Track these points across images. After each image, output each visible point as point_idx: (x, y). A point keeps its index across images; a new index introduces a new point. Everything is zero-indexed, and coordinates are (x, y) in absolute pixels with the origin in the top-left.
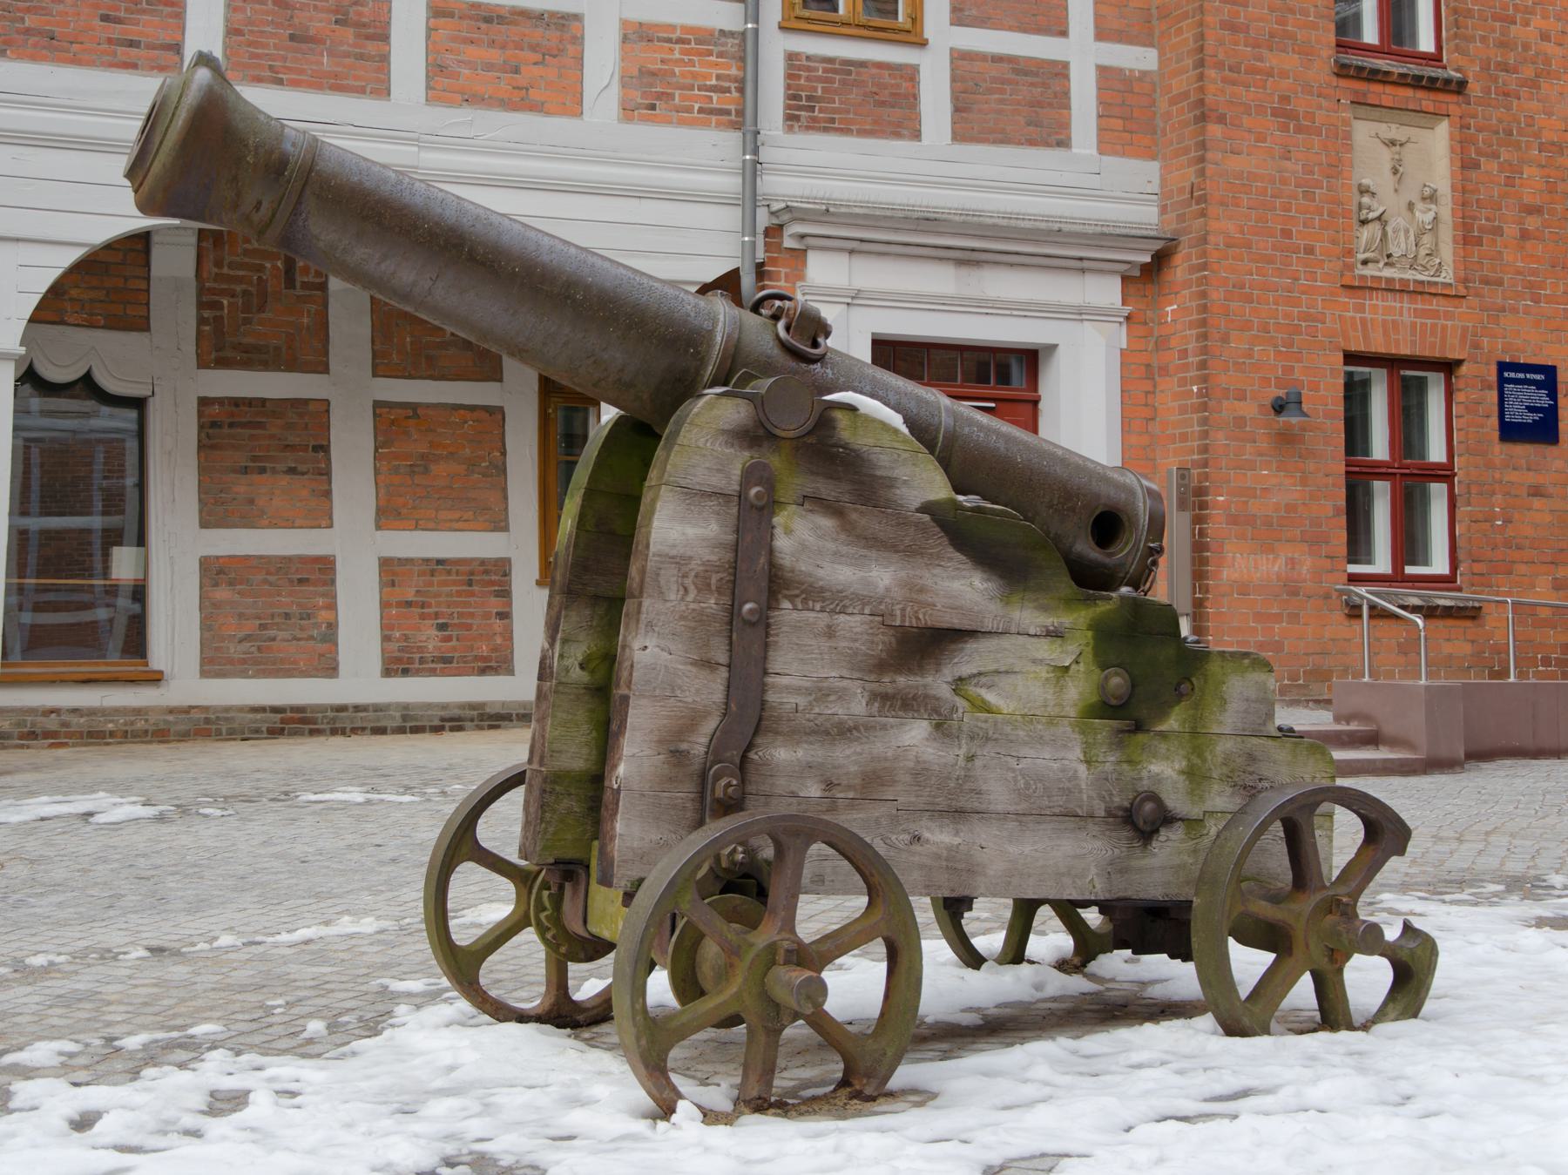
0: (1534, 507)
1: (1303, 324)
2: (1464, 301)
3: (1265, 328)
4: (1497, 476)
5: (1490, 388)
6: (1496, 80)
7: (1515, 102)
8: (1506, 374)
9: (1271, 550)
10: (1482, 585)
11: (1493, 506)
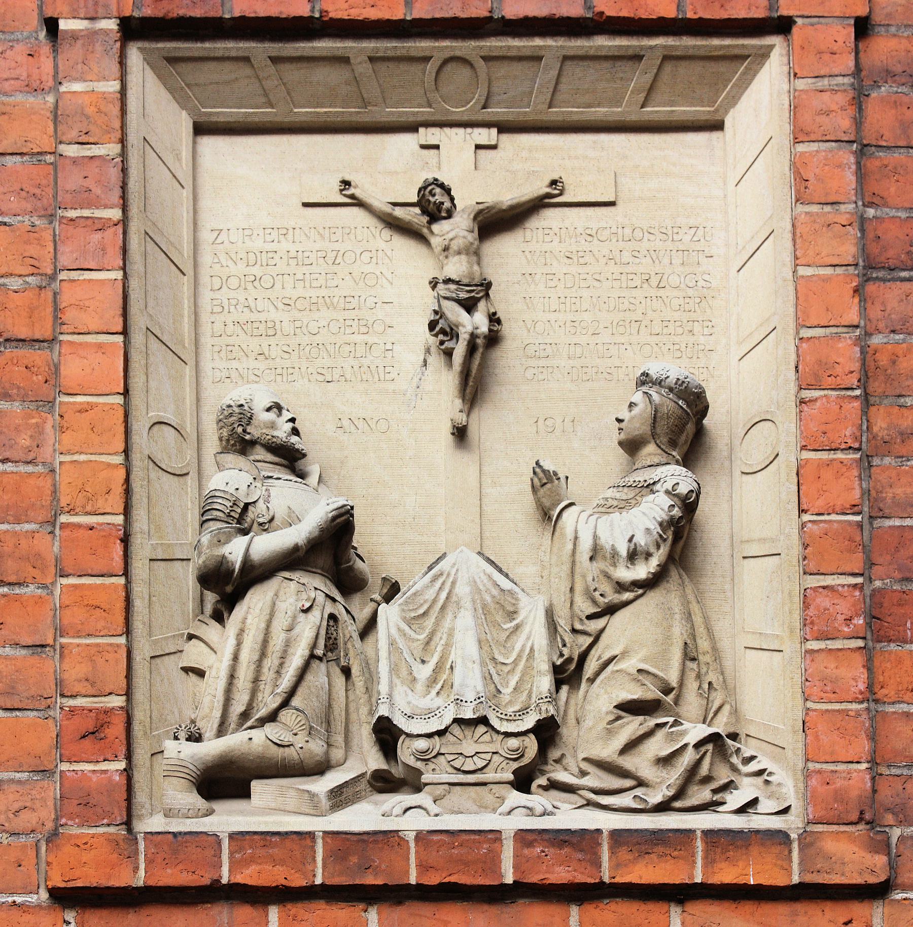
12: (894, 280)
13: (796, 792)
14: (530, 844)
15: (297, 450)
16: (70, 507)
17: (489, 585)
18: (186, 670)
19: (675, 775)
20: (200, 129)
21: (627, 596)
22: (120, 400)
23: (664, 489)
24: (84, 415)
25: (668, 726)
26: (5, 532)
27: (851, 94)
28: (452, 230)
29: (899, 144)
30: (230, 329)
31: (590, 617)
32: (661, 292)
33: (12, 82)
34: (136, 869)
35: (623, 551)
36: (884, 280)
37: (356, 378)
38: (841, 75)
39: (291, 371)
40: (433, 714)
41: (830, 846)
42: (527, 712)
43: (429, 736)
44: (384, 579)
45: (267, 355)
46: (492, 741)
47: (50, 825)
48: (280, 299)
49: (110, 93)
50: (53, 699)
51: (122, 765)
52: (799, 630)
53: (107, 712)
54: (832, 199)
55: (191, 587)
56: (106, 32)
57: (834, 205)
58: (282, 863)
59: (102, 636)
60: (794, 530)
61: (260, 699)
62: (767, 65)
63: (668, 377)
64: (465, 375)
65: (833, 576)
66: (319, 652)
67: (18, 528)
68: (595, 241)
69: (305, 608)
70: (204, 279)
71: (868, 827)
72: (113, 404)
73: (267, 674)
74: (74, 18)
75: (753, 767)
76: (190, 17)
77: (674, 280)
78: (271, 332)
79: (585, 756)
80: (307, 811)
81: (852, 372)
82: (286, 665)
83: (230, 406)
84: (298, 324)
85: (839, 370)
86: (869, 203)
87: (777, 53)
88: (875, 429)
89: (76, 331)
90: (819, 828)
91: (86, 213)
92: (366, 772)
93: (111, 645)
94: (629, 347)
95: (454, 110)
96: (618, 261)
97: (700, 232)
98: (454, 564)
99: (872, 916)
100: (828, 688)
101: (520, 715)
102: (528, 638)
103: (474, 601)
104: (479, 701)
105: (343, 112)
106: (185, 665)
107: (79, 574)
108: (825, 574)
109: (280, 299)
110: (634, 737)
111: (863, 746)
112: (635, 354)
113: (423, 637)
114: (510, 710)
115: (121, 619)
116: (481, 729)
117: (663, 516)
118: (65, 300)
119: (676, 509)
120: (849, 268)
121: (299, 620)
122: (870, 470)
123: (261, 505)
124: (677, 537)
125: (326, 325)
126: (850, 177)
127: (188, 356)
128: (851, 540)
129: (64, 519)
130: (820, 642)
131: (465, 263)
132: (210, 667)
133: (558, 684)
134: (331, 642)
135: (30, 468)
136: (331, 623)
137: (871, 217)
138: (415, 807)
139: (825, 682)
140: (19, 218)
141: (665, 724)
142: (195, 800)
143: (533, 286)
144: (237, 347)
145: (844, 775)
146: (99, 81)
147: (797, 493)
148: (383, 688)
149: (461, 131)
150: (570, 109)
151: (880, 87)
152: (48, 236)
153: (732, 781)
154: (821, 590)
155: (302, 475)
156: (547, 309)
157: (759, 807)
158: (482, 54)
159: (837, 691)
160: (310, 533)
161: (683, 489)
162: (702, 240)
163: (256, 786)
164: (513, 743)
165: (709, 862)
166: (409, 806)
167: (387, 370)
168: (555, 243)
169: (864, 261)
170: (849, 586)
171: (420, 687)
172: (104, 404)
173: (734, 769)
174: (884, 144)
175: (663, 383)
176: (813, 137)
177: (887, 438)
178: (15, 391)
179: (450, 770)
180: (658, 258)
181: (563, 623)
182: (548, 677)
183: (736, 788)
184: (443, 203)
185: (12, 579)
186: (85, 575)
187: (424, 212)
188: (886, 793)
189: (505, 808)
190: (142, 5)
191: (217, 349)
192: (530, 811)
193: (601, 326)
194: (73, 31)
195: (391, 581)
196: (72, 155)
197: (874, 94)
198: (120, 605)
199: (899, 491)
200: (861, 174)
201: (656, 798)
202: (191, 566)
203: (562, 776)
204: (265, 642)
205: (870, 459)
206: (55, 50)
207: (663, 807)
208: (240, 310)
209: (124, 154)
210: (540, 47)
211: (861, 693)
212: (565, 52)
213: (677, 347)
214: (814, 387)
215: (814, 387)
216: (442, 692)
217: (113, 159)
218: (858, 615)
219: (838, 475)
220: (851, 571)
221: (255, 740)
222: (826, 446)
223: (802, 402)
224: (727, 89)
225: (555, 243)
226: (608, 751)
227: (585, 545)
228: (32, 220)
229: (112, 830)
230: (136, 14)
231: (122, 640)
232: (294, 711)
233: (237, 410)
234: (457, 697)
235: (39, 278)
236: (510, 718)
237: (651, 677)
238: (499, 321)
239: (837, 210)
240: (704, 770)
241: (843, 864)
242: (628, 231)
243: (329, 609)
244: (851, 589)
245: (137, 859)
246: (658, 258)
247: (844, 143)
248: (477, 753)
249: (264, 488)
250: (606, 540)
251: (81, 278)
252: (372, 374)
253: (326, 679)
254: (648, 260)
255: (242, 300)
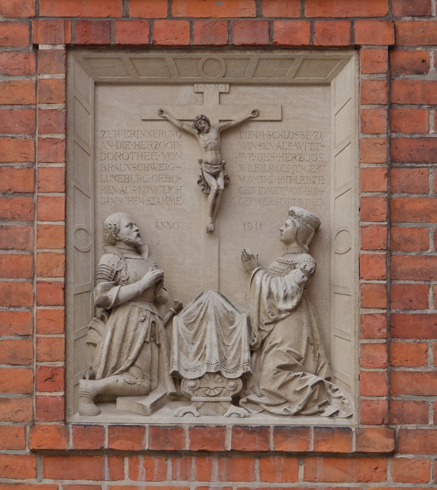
12: (403, 167)
13: (355, 408)
14: (238, 433)
15: (139, 244)
16: (42, 273)
17: (222, 309)
18: (88, 343)
20: (96, 84)
21: (283, 315)
23: (300, 267)
24: (47, 230)
25: (300, 377)
26: (12, 282)
27: (386, 82)
28: (209, 140)
29: (407, 103)
30: (109, 178)
31: (266, 324)
32: (301, 163)
33: (17, 71)
34: (68, 441)
35: (282, 295)
36: (399, 167)
37: (164, 203)
38: (382, 73)
39: (135, 199)
40: (197, 369)
41: (370, 435)
42: (238, 369)
43: (195, 379)
44: (176, 302)
45: (125, 191)
46: (223, 381)
48: (131, 165)
49: (61, 79)
50: (32, 360)
51: (62, 394)
52: (358, 333)
54: (377, 132)
55: (91, 304)
56: (59, 51)
57: (378, 135)
59: (54, 334)
60: (357, 285)
61: (121, 361)
62: (349, 63)
63: (303, 215)
64: (214, 207)
65: (373, 309)
66: (148, 340)
67: (18, 280)
68: (272, 138)
69: (142, 320)
71: (386, 426)
72: (60, 225)
73: (124, 349)
74: (46, 44)
76: (96, 44)
78: (127, 180)
79: (263, 388)
80: (141, 413)
81: (384, 214)
82: (133, 346)
83: (110, 224)
84: (139, 177)
85: (378, 212)
86: (393, 130)
87: (354, 59)
88: (394, 238)
89: (44, 191)
91: (50, 136)
92: (167, 393)
93: (58, 338)
94: (286, 189)
95: (210, 78)
96: (282, 148)
97: (319, 135)
98: (207, 299)
99: (387, 465)
100: (370, 362)
101: (235, 370)
102: (239, 334)
103: (215, 316)
104: (217, 364)
105: (161, 78)
106: (88, 341)
107: (44, 304)
108: (370, 308)
109: (131, 165)
110: (285, 381)
111: (384, 389)
112: (289, 193)
113: (193, 332)
115: (62, 326)
116: (218, 376)
119: (305, 277)
120: (383, 164)
121: (139, 326)
122: (391, 257)
123: (123, 272)
125: (151, 177)
127: (91, 195)
128: (382, 293)
130: (367, 340)
131: (214, 154)
132: (99, 342)
133: (252, 353)
134: (153, 333)
135: (23, 253)
136: (153, 325)
137: (394, 137)
138: (189, 413)
139: (369, 358)
140: (20, 135)
141: (298, 376)
143: (244, 159)
144: (112, 187)
145: (376, 402)
146: (56, 74)
147: (358, 268)
149: (213, 86)
150: (262, 78)
151: (399, 75)
153: (327, 401)
154: (368, 316)
156: (250, 171)
157: (339, 414)
158: (224, 58)
159: (374, 363)
160: (144, 286)
162: (320, 138)
163: (119, 400)
164: (232, 383)
166: (186, 412)
167: (178, 199)
168: (254, 139)
169: (390, 158)
170: (380, 314)
171: (191, 356)
172: (57, 225)
173: (329, 395)
174: (401, 103)
175: (301, 217)
176: (369, 102)
177: (399, 242)
178: (17, 216)
179: (204, 395)
180: (300, 147)
181: (255, 326)
182: (248, 353)
183: (329, 405)
184: (205, 127)
185: (15, 304)
186: (47, 305)
189: (229, 412)
190: (75, 38)
191: (103, 188)
192: (239, 416)
193: (274, 179)
194: (45, 50)
195: (179, 303)
196: (44, 109)
197: (396, 79)
198: (62, 319)
199: (403, 267)
200: (390, 118)
201: (294, 410)
202: (91, 294)
203: (253, 397)
205: (391, 252)
207: (297, 414)
208: (113, 170)
209: (66, 108)
210: (249, 55)
211: (384, 364)
212: (260, 57)
213: (307, 189)
214: (367, 220)
215: (367, 220)
216: (201, 359)
217: (61, 111)
218: (384, 328)
220: (381, 307)
221: (119, 381)
222: (372, 248)
223: (362, 227)
224: (332, 71)
225: (254, 139)
226: (274, 387)
228: (25, 136)
229: (58, 423)
230: (72, 42)
231: (63, 336)
232: (136, 368)
233: (113, 227)
234: (207, 362)
235: (28, 163)
236: (231, 371)
237: (292, 354)
238: (228, 179)
239: (379, 137)
241: (375, 443)
242: (287, 134)
243: (152, 320)
244: (381, 315)
245: (69, 437)
246: (300, 147)
247: (382, 105)
248: (216, 387)
249: (125, 263)
251: (47, 166)
252: (171, 201)
253: (150, 351)
254: (296, 147)
255: (114, 165)
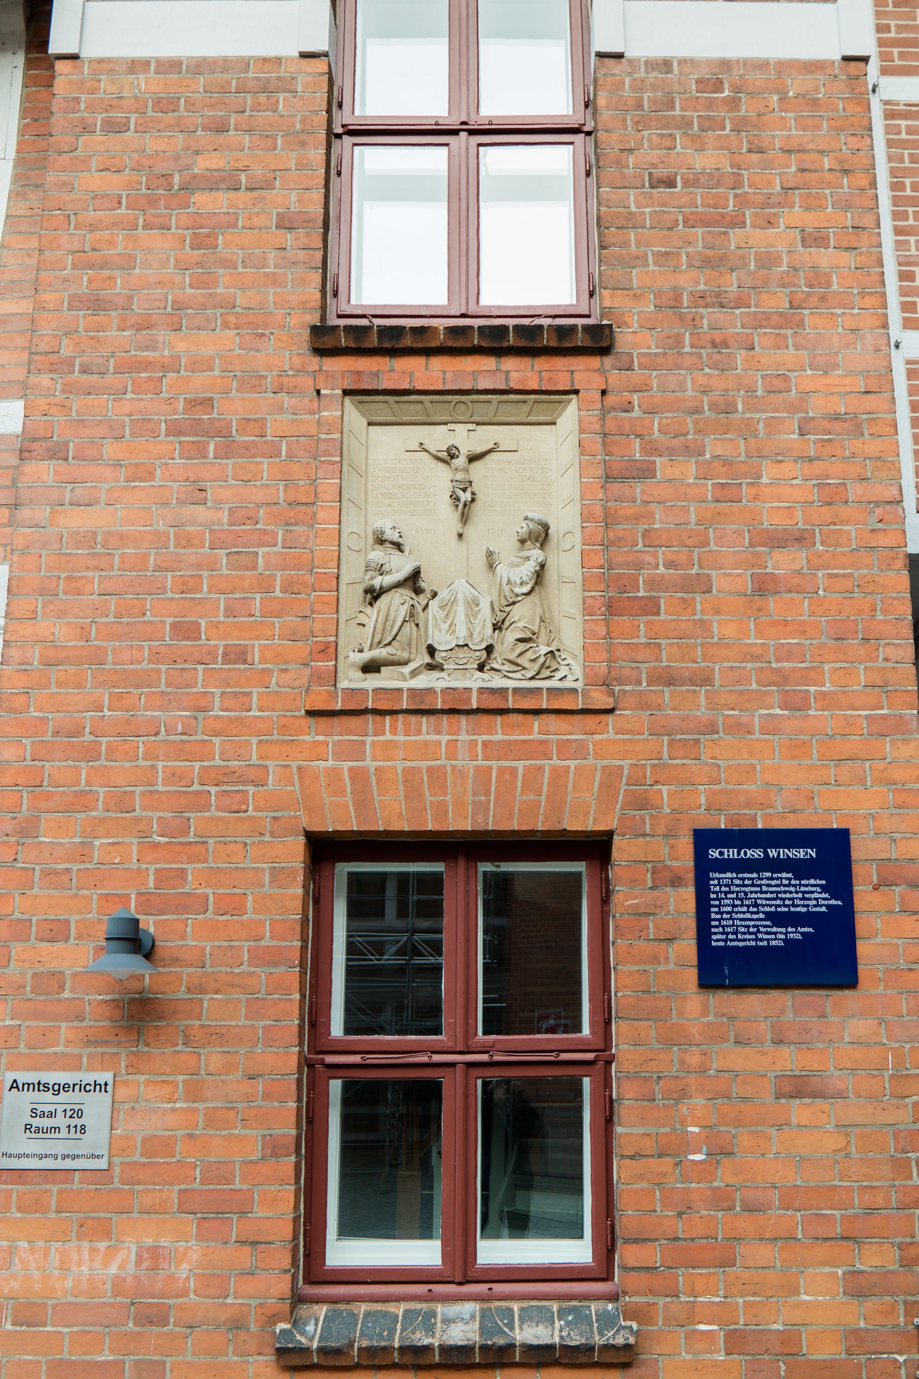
0: (794, 1120)
1: (213, 790)
2: (610, 718)
3: (122, 803)
4: (694, 1060)
5: (676, 881)
6: (694, 321)
7: (741, 356)
8: (714, 854)
9: (103, 1230)
10: (652, 1292)
11: (683, 1123)
14: (482, 693)
19: (536, 666)
20: (369, 424)
21: (520, 598)
22: (339, 481)
47: (306, 685)
51: (333, 663)
53: (329, 643)
58: (391, 700)
64: (463, 514)
70: (370, 478)
75: (566, 662)
77: (539, 479)
90: (589, 687)
91: (328, 458)
114: (476, 641)
116: (466, 648)
117: (532, 570)
118: (319, 489)
124: (538, 576)
126: (600, 446)
129: (315, 570)
133: (494, 630)
142: (360, 674)
148: (430, 633)
152: (314, 466)
155: (402, 552)
161: (540, 560)
163: (382, 668)
164: (478, 654)
165: (548, 700)
171: (443, 632)
173: (558, 663)
187: (449, 455)
188: (614, 674)
189: (474, 678)
192: (484, 680)
199: (618, 559)
200: (604, 444)
201: (529, 675)
203: (495, 666)
204: (387, 616)
206: (319, 400)
207: (532, 678)
219: (596, 554)
226: (512, 657)
227: (505, 581)
240: (547, 664)
243: (412, 602)
250: (512, 579)
